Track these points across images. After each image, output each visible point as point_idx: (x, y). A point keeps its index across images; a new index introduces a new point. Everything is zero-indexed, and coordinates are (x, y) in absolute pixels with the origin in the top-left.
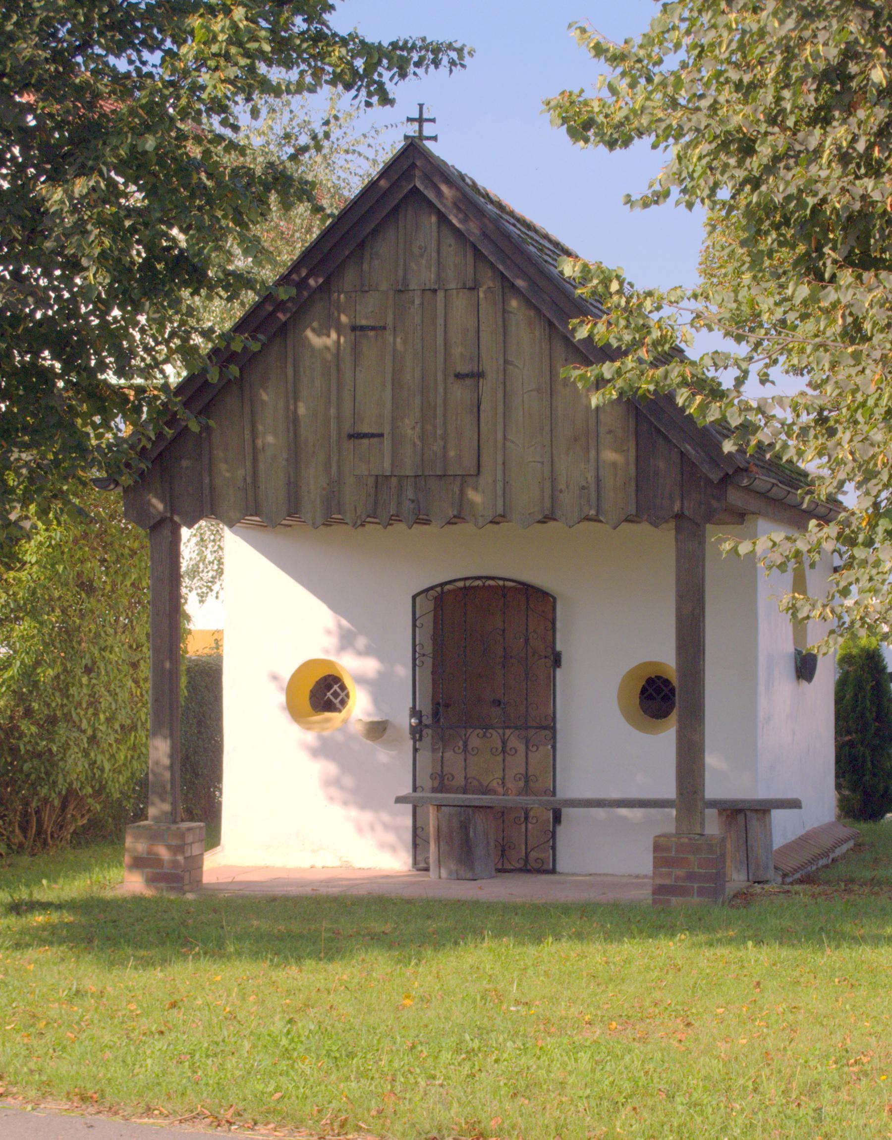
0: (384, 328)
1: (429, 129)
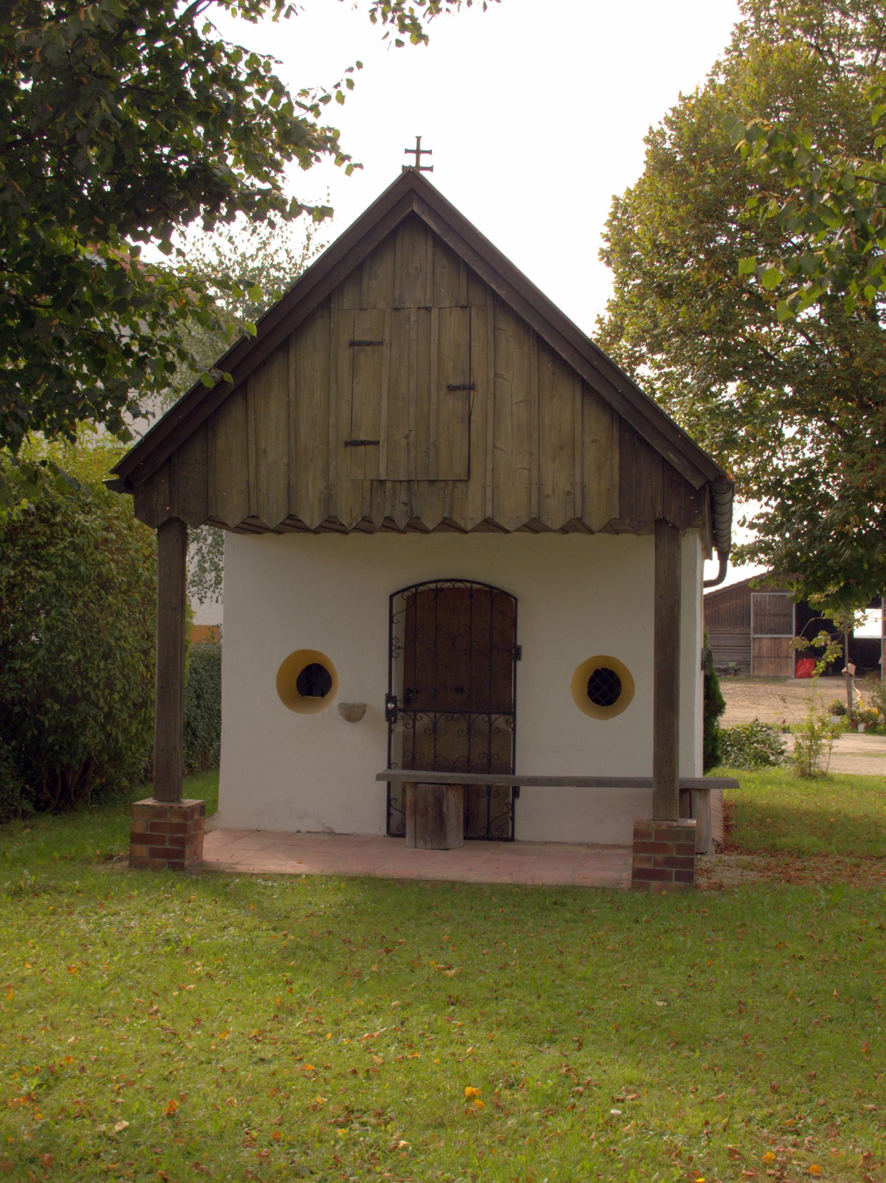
0: (381, 343)
1: (425, 161)
